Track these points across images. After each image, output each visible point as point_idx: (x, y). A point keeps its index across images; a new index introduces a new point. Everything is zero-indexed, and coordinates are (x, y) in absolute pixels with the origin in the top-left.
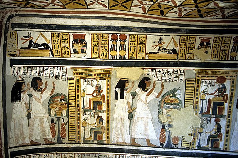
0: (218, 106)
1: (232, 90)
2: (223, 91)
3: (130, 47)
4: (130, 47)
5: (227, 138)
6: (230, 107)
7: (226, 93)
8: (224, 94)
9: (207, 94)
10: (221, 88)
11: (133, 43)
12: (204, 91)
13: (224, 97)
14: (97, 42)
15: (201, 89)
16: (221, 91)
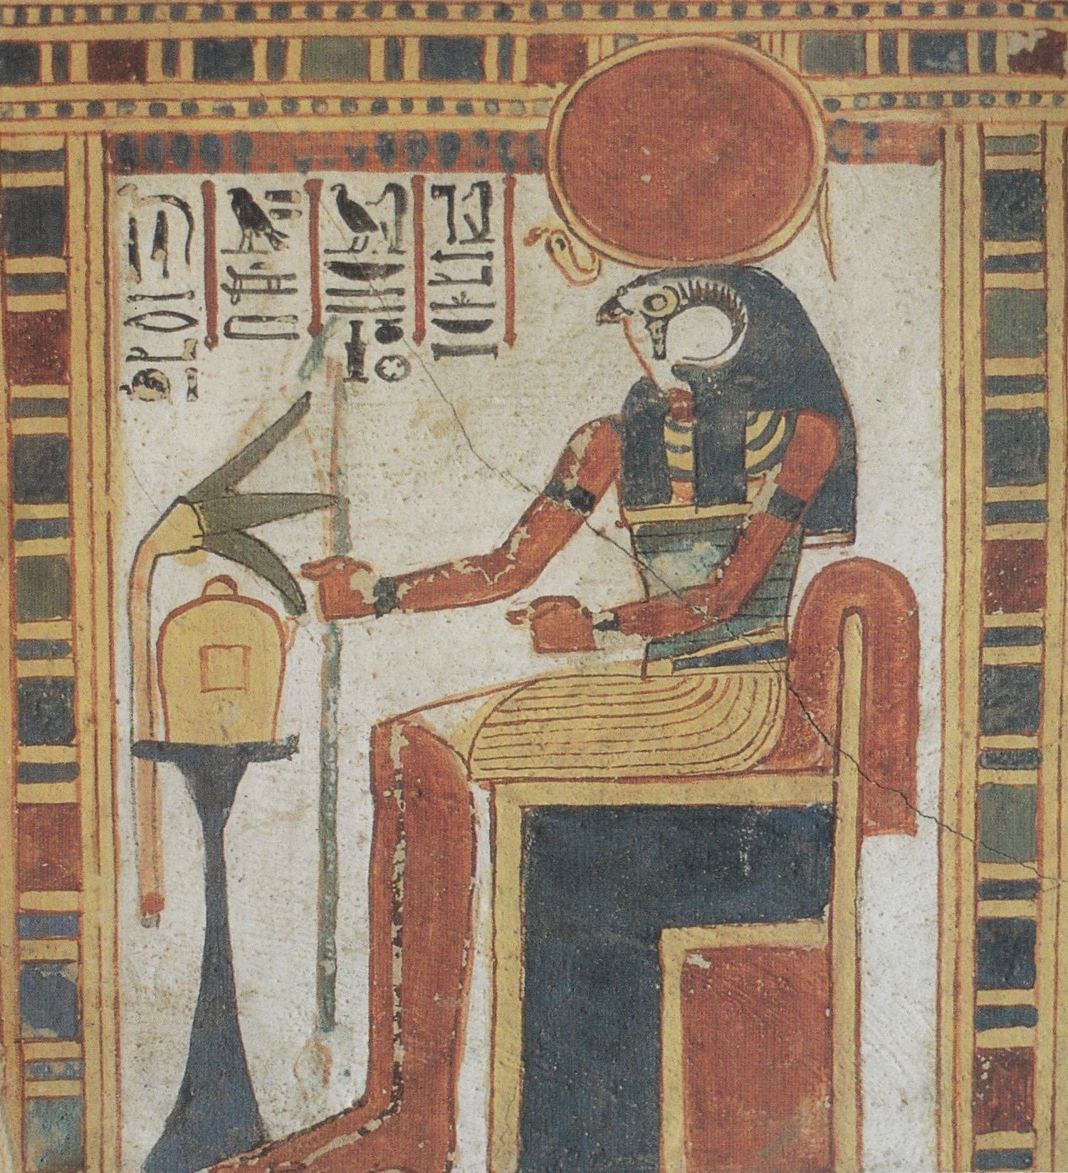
0: (680, 945)
1: (1013, 446)
2: (760, 496)
5: (1010, 890)
6: (1005, 952)
7: (865, 546)
8: (812, 563)
9: (335, 572)
10: (709, 396)
12: (225, 514)
13: (804, 664)
15: (158, 450)
16: (720, 471)
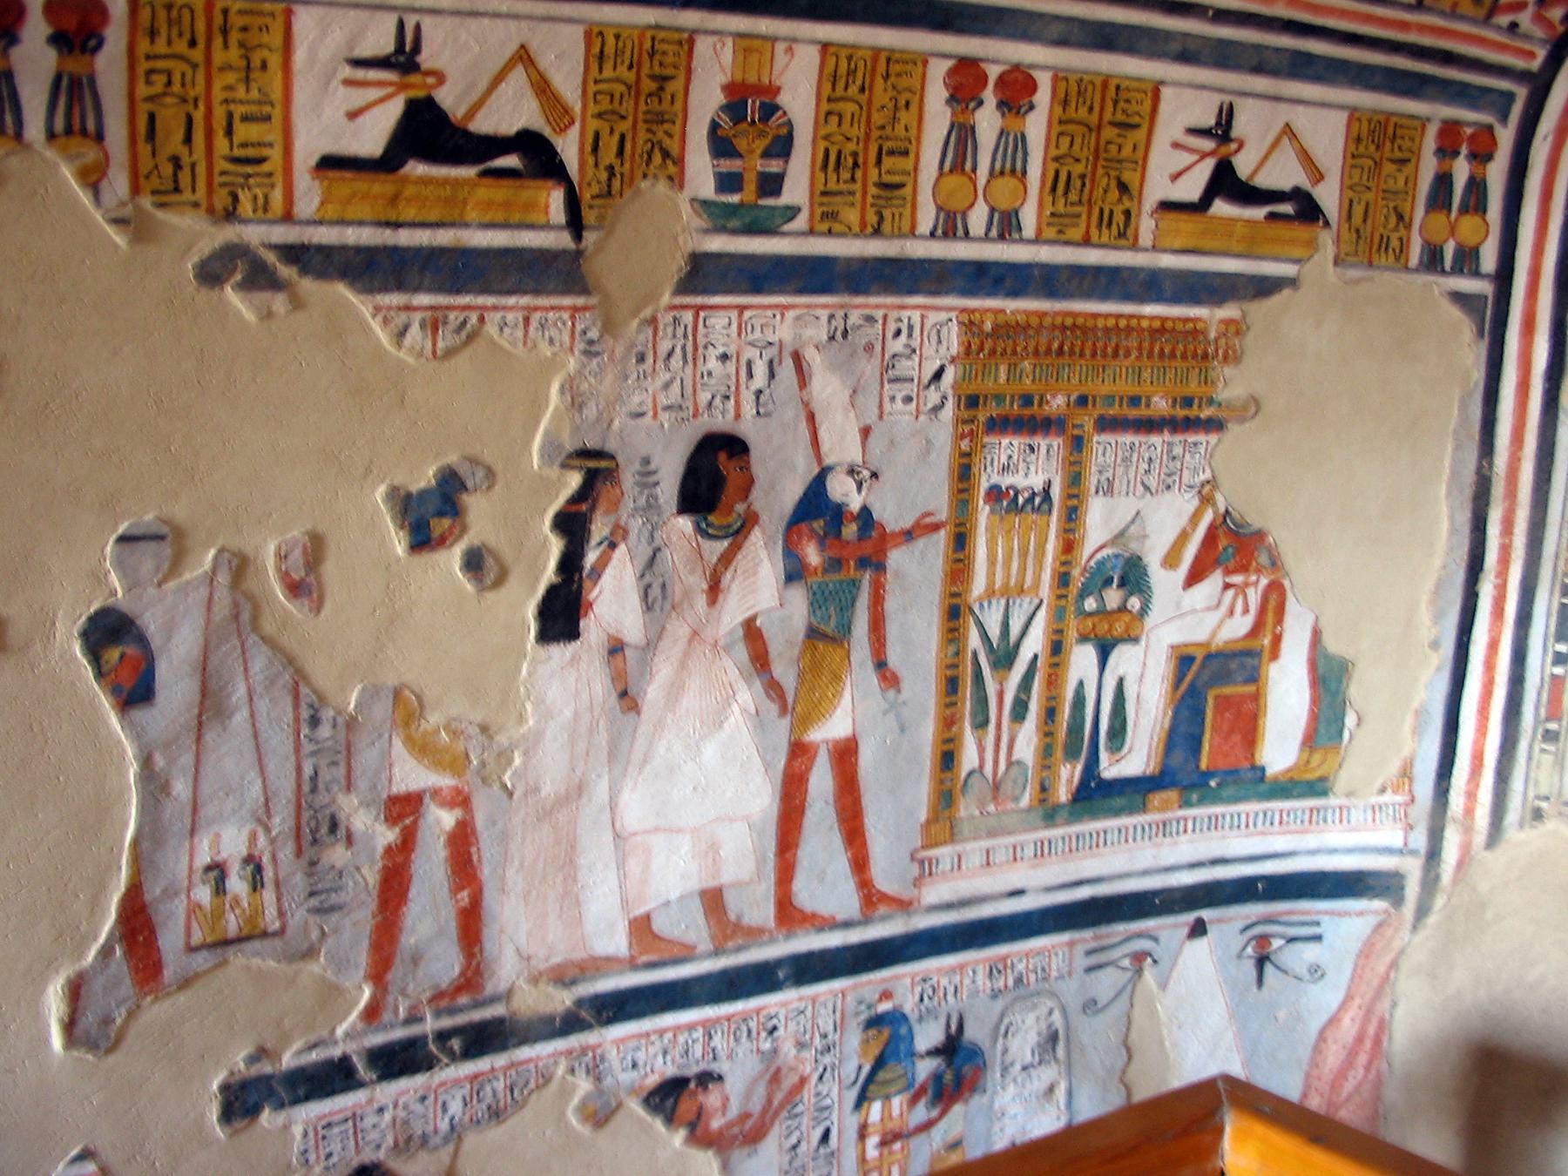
3: (143, 109)
4: (143, 109)
11: (169, 74)
14: (178, 67)
